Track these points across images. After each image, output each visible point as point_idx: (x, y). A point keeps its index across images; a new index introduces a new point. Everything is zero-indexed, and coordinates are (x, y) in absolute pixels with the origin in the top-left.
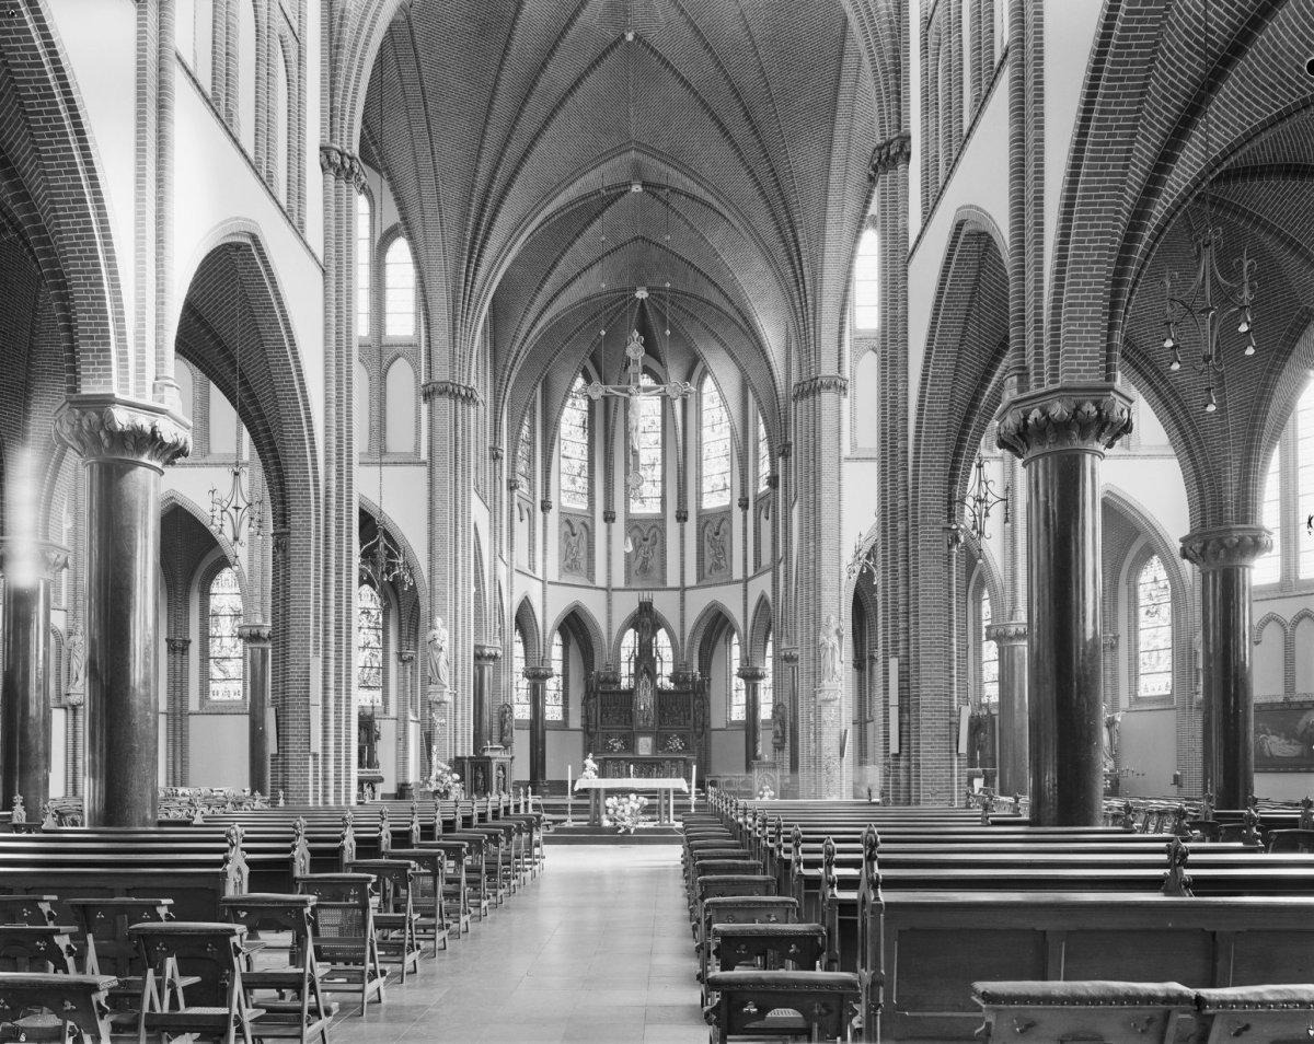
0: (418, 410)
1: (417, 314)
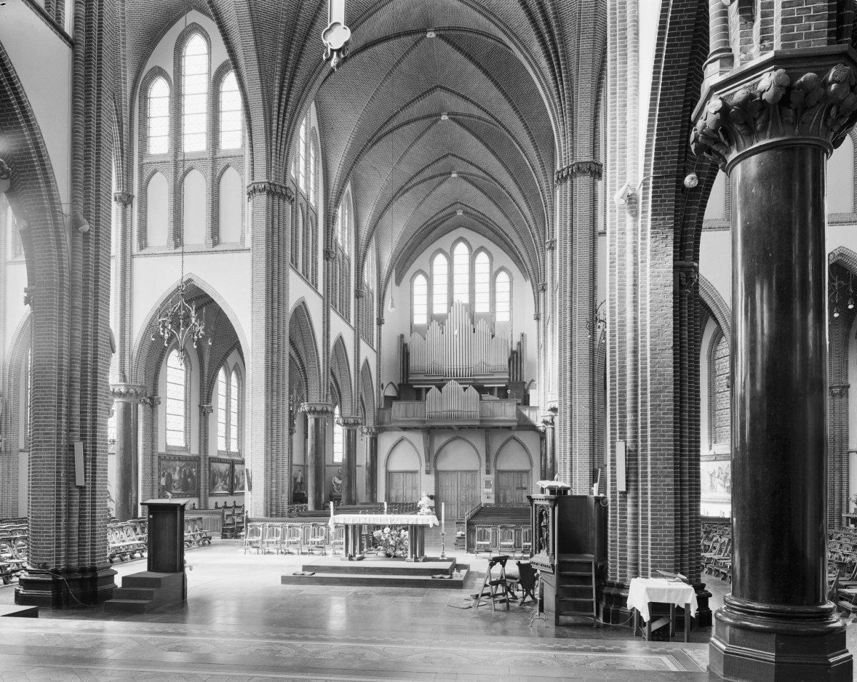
0: (243, 206)
1: (243, 130)
